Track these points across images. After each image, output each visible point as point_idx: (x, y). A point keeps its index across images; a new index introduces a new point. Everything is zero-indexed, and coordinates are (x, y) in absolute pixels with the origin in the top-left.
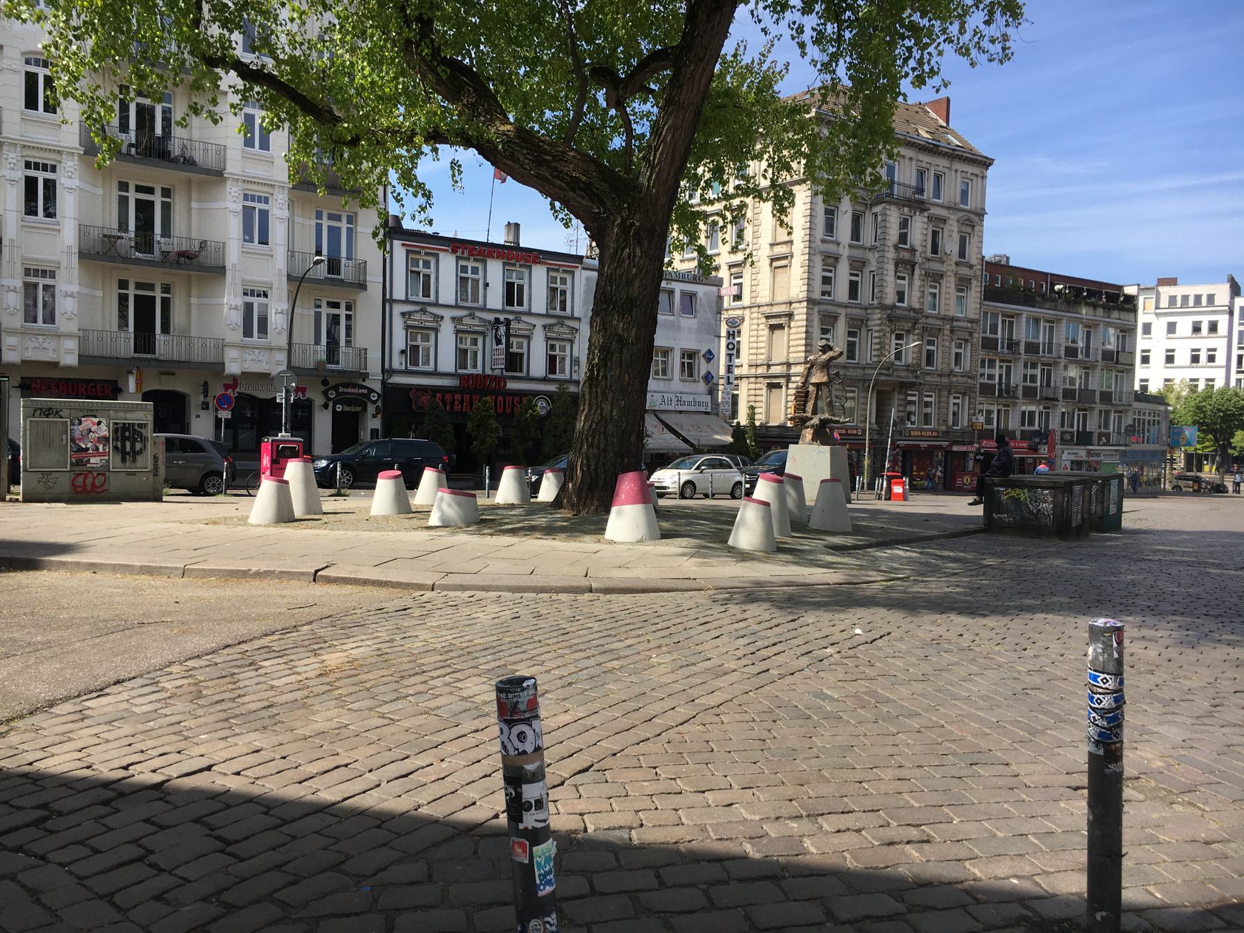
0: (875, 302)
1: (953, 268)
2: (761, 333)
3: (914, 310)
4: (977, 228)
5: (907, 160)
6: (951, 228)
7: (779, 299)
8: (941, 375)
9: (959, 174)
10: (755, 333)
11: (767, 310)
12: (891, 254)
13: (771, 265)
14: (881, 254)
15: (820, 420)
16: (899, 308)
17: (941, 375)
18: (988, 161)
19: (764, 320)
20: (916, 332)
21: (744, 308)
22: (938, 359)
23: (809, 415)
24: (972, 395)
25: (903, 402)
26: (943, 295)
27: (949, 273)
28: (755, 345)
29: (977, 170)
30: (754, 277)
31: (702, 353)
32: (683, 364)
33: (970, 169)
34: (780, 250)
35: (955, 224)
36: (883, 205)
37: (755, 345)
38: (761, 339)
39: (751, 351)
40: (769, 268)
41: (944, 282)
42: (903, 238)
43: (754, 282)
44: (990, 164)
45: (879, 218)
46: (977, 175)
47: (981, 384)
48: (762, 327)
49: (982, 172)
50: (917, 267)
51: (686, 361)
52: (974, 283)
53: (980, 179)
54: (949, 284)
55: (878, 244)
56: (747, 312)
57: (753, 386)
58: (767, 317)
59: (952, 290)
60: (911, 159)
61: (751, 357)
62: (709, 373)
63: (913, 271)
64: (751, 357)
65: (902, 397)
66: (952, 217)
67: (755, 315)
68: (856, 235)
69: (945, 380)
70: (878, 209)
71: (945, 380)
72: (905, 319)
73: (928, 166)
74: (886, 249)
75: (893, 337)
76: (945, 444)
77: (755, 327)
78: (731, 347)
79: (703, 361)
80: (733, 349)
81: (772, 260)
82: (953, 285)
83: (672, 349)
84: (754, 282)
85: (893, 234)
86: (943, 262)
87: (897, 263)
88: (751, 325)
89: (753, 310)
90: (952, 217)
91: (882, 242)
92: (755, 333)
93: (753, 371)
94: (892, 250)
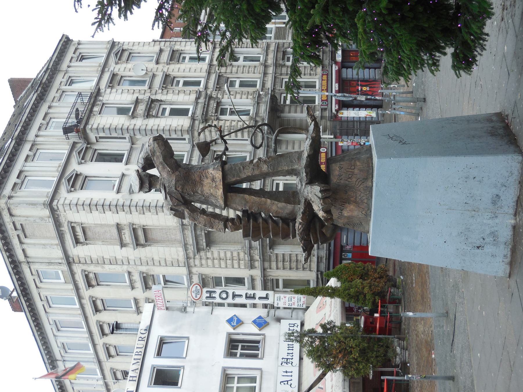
0: (187, 136)
1: (160, 66)
2: (216, 255)
3: (197, 98)
4: (125, 47)
5: (51, 111)
6: (122, 69)
7: (179, 236)
8: (265, 74)
9: (72, 64)
10: (216, 262)
11: (191, 249)
12: (139, 122)
13: (143, 246)
14: (137, 133)
15: (310, 182)
16: (194, 113)
17: (265, 74)
18: (64, 39)
19: (202, 253)
20: (220, 96)
21: (190, 273)
22: (248, 77)
23: (301, 208)
24: (286, 46)
25: (293, 108)
26: (187, 74)
27: (165, 70)
28: (229, 262)
29: (72, 49)
30: (157, 263)
31: (231, 330)
32: (242, 356)
33: (70, 54)
34: (127, 237)
35: (118, 66)
36: (88, 131)
37: (229, 262)
38: (222, 255)
39: (236, 265)
40: (148, 248)
41: (173, 74)
42: (122, 111)
43: (163, 263)
44: (67, 38)
45: (102, 134)
46: (76, 49)
47: (275, 38)
48: (209, 255)
49: (74, 45)
50: (153, 97)
51: (239, 351)
52: (177, 47)
53: (80, 46)
54: (174, 69)
55: (127, 136)
56: (194, 270)
57: (274, 265)
58: (199, 250)
59: (182, 66)
60: (50, 107)
61: (242, 266)
62: (254, 322)
63: (157, 101)
64: (242, 266)
65: (287, 109)
66: (112, 69)
67: (197, 262)
68: (116, 158)
69: (271, 70)
70: (92, 136)
71: (271, 70)
72: (206, 107)
73: (59, 91)
74: (131, 127)
75: (222, 117)
76: (335, 68)
77: (210, 262)
78: (224, 295)
79: (240, 330)
80: (227, 293)
81: (138, 244)
82: (178, 66)
83: (224, 370)
84: (163, 263)
85: (122, 121)
86: (154, 76)
87: (148, 115)
88: (208, 266)
89: (192, 264)
90: (112, 69)
91: (125, 132)
92: (216, 262)
93: (257, 264)
94: (134, 121)
